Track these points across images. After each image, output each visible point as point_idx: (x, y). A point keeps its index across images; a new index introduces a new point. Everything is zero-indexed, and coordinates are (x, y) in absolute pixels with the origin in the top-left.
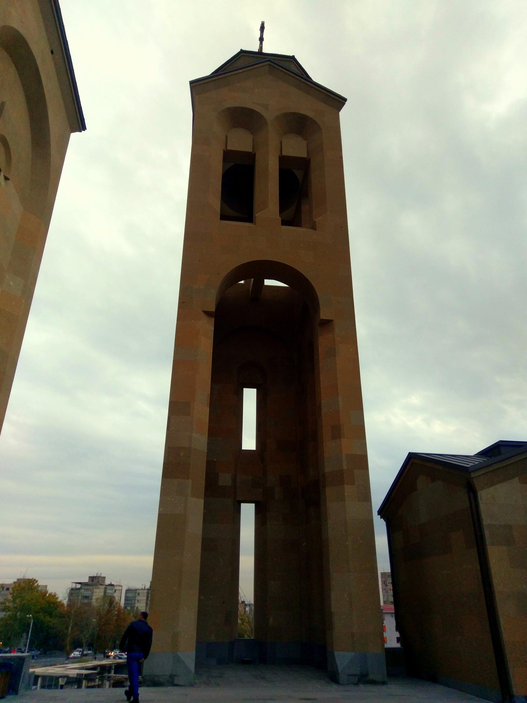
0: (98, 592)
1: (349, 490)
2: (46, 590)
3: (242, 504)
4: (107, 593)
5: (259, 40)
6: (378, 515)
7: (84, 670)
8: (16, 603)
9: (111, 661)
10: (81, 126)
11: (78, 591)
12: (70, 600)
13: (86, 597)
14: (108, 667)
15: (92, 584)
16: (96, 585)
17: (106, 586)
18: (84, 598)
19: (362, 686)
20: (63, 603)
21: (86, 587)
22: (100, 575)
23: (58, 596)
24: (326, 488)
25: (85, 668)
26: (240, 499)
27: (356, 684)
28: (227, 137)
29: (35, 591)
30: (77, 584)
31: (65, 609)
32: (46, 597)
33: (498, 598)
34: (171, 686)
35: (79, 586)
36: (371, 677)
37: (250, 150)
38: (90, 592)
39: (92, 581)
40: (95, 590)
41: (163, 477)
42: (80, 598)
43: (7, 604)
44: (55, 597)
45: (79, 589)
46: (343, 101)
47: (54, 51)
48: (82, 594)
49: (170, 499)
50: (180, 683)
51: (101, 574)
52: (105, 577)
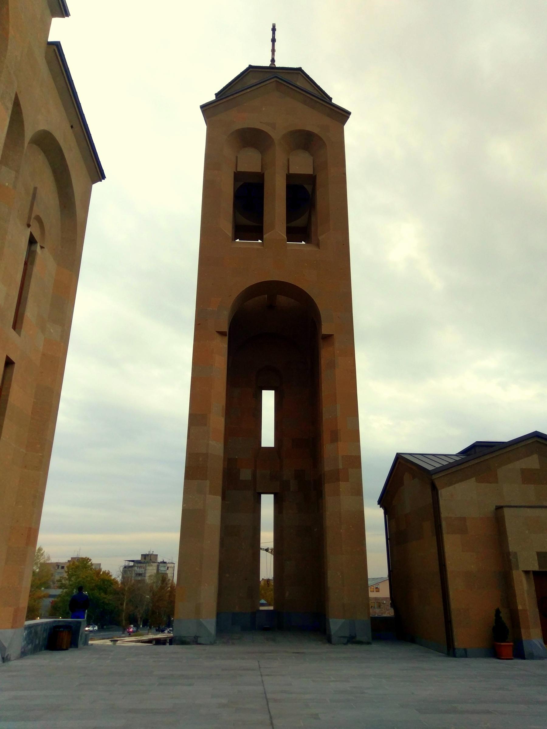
0: (151, 570)
1: (343, 486)
2: (100, 568)
3: (262, 495)
4: (159, 571)
5: (271, 42)
6: (378, 504)
7: (140, 643)
8: (72, 581)
9: (166, 635)
10: (100, 175)
11: (131, 569)
12: (123, 577)
13: (140, 575)
14: (163, 640)
15: (144, 561)
16: (148, 562)
17: (159, 564)
18: (138, 575)
19: (350, 645)
20: (117, 580)
21: (138, 564)
22: (152, 553)
23: (112, 574)
24: (325, 484)
25: (141, 641)
26: (260, 491)
27: (345, 644)
28: (237, 157)
29: (89, 570)
30: (130, 562)
31: (119, 586)
32: (100, 575)
33: (449, 575)
34: (195, 644)
35: (132, 564)
36: (358, 638)
37: (259, 171)
38: (142, 570)
39: (145, 559)
40: (148, 568)
41: (185, 479)
42: (134, 575)
43: (63, 582)
44: (109, 575)
45: (132, 567)
46: (347, 115)
47: (73, 126)
48: (136, 572)
49: (191, 497)
50: (202, 642)
51: (153, 552)
52: (157, 555)
